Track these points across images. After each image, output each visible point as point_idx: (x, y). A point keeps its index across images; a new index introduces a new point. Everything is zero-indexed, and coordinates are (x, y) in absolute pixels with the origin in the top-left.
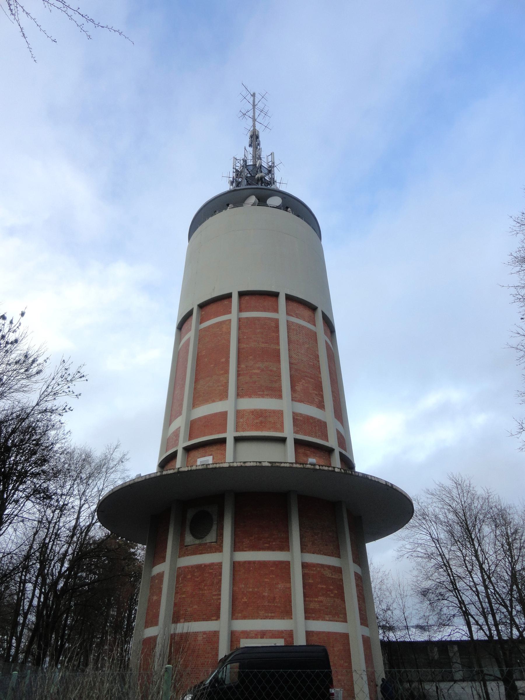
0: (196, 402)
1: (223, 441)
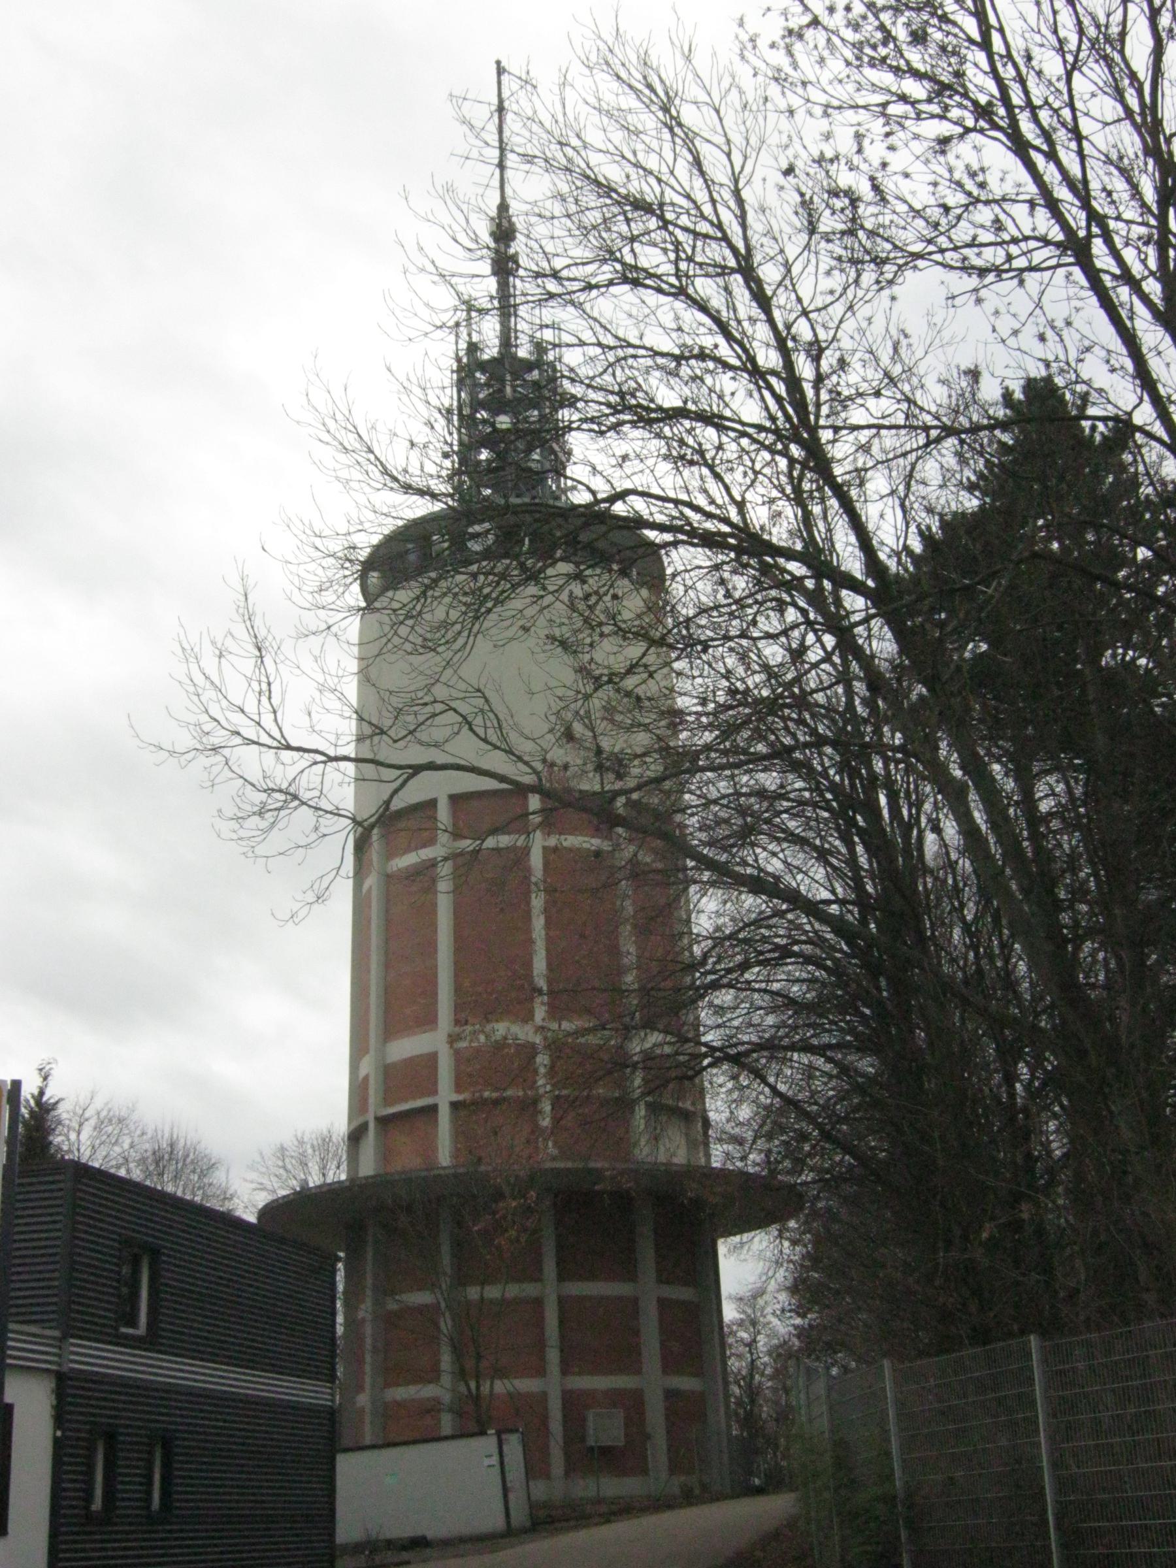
0: (390, 1031)
1: (433, 1109)
